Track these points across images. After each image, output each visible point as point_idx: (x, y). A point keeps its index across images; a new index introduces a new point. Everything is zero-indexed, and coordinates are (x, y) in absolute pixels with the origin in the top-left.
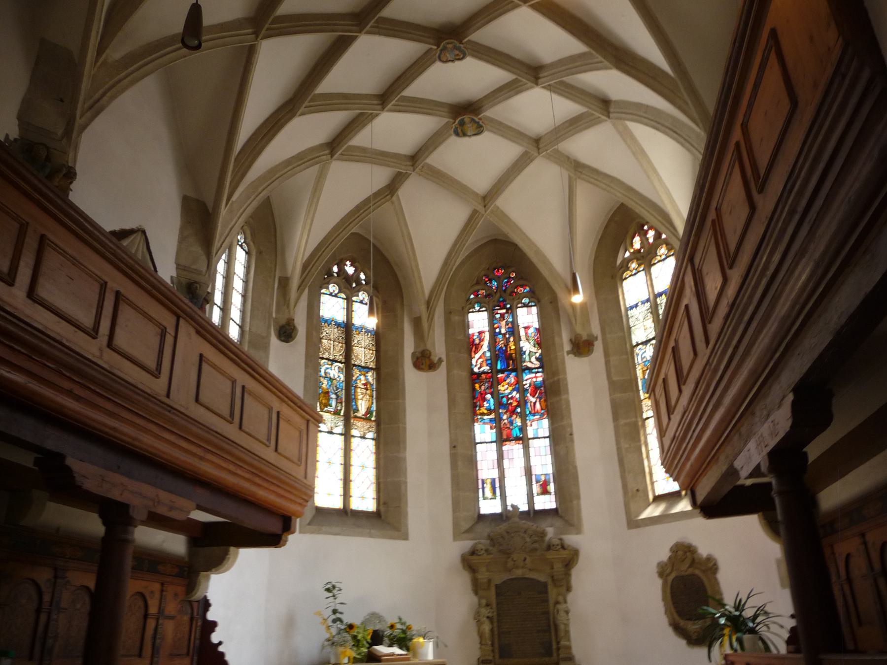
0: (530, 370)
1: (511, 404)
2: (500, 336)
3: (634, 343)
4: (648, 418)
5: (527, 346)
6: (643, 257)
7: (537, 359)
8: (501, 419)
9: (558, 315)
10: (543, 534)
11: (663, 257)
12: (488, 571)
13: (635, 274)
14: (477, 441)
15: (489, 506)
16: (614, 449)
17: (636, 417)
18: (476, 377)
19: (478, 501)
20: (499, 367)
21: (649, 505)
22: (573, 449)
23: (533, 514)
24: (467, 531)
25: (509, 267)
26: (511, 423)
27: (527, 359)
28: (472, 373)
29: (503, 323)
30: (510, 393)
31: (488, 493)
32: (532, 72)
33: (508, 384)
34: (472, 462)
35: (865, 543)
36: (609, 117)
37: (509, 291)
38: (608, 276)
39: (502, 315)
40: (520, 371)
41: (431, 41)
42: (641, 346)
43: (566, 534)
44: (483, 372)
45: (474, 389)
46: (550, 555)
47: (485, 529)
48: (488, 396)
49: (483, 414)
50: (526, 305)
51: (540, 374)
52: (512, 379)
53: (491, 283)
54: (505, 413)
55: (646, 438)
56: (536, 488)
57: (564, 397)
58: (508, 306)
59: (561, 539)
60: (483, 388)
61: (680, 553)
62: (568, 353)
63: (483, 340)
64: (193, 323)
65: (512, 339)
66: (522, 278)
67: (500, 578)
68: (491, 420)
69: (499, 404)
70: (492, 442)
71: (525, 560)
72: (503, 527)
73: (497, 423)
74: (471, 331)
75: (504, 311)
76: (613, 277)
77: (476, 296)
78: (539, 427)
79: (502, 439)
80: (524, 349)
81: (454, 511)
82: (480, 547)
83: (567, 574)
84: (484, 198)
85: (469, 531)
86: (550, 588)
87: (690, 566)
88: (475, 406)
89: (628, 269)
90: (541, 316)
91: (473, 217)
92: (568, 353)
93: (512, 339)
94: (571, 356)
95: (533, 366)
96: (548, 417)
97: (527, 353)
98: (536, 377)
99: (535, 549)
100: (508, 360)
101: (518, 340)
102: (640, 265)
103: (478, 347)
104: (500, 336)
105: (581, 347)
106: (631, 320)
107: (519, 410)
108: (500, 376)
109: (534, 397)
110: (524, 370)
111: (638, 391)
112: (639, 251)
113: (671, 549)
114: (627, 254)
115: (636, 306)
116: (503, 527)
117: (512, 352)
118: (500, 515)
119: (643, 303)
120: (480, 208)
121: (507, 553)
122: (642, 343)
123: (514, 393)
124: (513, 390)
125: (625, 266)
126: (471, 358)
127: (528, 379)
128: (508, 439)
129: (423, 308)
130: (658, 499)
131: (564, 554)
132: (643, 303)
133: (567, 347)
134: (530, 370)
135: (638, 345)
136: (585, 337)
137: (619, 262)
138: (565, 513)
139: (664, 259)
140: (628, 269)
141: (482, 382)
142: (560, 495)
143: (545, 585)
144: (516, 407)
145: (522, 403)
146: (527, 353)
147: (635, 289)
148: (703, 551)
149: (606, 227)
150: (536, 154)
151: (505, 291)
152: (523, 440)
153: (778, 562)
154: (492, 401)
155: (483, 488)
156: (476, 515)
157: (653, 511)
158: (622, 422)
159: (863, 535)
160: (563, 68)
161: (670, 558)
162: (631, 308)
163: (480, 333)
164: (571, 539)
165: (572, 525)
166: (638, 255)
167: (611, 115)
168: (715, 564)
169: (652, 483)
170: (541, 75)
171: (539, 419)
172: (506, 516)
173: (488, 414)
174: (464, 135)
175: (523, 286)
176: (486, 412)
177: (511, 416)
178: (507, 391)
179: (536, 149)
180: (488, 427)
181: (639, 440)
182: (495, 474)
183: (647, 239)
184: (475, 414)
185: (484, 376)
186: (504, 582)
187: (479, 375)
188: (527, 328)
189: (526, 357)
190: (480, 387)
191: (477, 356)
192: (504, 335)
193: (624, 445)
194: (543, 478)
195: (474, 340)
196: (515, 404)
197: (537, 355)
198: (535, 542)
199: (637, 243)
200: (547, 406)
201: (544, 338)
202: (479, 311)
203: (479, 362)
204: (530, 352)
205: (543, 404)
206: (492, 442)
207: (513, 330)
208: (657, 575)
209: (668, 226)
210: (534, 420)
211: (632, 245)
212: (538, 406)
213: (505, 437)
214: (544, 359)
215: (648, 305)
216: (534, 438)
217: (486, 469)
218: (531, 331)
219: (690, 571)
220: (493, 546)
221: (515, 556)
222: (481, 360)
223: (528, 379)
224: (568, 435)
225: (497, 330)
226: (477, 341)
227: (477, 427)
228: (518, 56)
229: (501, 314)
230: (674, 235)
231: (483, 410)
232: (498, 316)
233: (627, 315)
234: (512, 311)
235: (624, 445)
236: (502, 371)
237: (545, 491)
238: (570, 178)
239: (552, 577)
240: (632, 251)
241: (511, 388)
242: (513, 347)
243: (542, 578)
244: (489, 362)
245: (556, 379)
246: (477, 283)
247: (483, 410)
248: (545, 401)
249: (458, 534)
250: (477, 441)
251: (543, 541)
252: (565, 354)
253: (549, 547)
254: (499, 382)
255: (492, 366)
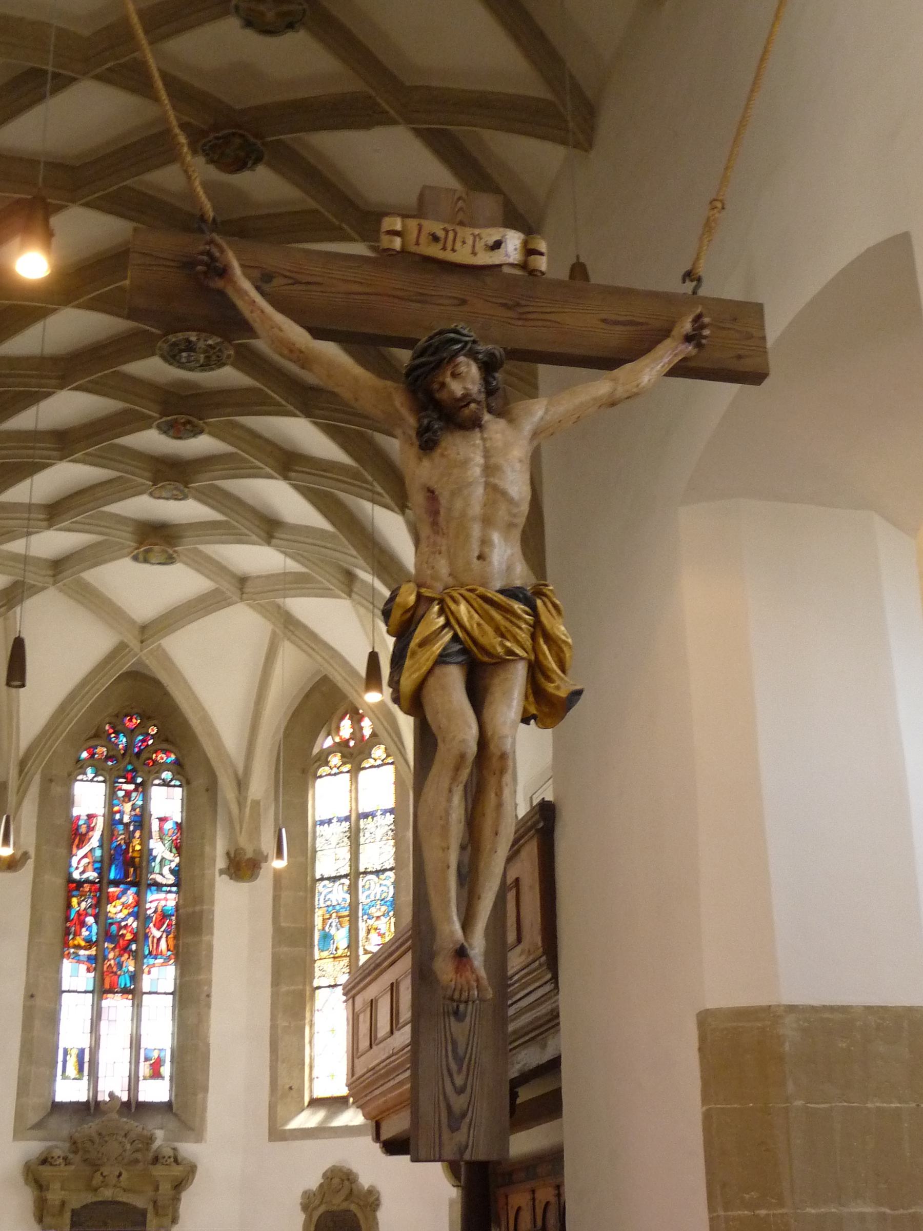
0: (158, 886)
1: (123, 936)
2: (121, 827)
3: (318, 876)
4: (319, 988)
5: (159, 849)
6: (352, 754)
7: (172, 871)
8: (105, 958)
9: (215, 812)
10: (151, 1139)
11: (379, 762)
12: (62, 1188)
13: (335, 774)
14: (64, 988)
15: (70, 1090)
16: (268, 1024)
17: (304, 985)
18: (74, 886)
19: (55, 1080)
20: (112, 876)
21: (303, 1110)
22: (208, 1020)
23: (134, 1108)
24: (34, 1127)
25: (149, 718)
26: (120, 965)
27: (157, 870)
28: (70, 880)
29: (127, 807)
30: (123, 919)
31: (72, 1070)
32: (270, 528)
33: (123, 904)
34: (53, 1019)
35: (534, 1199)
36: (350, 596)
37: (144, 756)
38: (298, 767)
39: (128, 794)
40: (143, 886)
41: (147, 474)
42: (326, 882)
43: (181, 1141)
44: (87, 881)
45: (69, 906)
46: (158, 1171)
47: (64, 1127)
48: (90, 920)
49: (79, 947)
50: (166, 784)
51: (173, 896)
52: (130, 897)
53: (117, 737)
54: (113, 949)
55: (312, 1015)
56: (144, 1069)
57: (205, 938)
58: (139, 780)
59: (175, 1149)
60: (83, 905)
61: (336, 1181)
62: (222, 872)
63: (93, 829)
64: (133, 1067)
65: (137, 834)
66: (167, 740)
67: (80, 1199)
68: (89, 958)
69: (107, 935)
70: (86, 992)
71: (120, 1175)
72: (92, 1127)
73: (96, 963)
74: (76, 812)
75: (131, 787)
76: (304, 771)
77: (92, 755)
78: (161, 977)
79: (103, 988)
80: (154, 853)
81: (19, 1095)
82: (57, 1153)
83: (176, 1199)
84: (144, 628)
85: (39, 1125)
86: (150, 1215)
87: (346, 1199)
88: (67, 932)
89: (326, 763)
90: (189, 804)
91: (120, 649)
92: (222, 872)
93: (137, 834)
94: (225, 877)
95: (164, 881)
96: (176, 963)
97: (158, 860)
98: (166, 899)
99: (137, 1161)
100: (126, 864)
101: (146, 836)
102: (344, 763)
103: (82, 839)
104: (121, 827)
105: (243, 867)
106: (318, 841)
107: (134, 947)
108: (111, 890)
109: (159, 929)
110: (150, 886)
111: (312, 946)
112: (348, 741)
113: (324, 1175)
114: (329, 742)
115: (329, 822)
116: (92, 1127)
117: (135, 855)
118: (127, 1105)
119: (340, 820)
120: (134, 644)
121: (95, 1165)
122: (329, 879)
123: (130, 920)
124: (130, 914)
125: (323, 759)
126: (71, 855)
127: (156, 901)
128: (111, 991)
129: (13, 772)
130: (316, 1103)
131: (177, 1171)
132: (340, 820)
133: (221, 863)
134: (158, 886)
135: (322, 879)
136: (249, 854)
137: (316, 750)
138: (183, 1111)
139: (378, 766)
140: (326, 763)
141: (82, 896)
142: (180, 1081)
143: (144, 1213)
144: (130, 941)
145: (141, 937)
146: (158, 860)
147: (329, 794)
148: (365, 1181)
149: (307, 696)
150: (235, 598)
151: (138, 755)
152: (133, 992)
153: (452, 1203)
154: (95, 928)
155: (65, 1062)
156: (50, 1104)
157: (308, 1119)
158: (284, 988)
159: (533, 1192)
160: (310, 541)
161: (321, 1185)
162: (322, 823)
163: (90, 817)
164: (188, 1149)
165: (191, 1129)
166: (345, 750)
167: (354, 595)
168: (378, 1199)
169: (311, 1080)
170: (276, 535)
171: (162, 965)
172: (89, 1109)
173: (85, 948)
174: (146, 561)
175: (167, 752)
176: (83, 943)
177: (121, 955)
178: (121, 915)
179: (239, 593)
180: (83, 968)
181: (304, 1018)
182: (85, 1042)
183: (362, 728)
184: (66, 944)
185: (87, 887)
186: (85, 1207)
187: (80, 884)
188: (162, 820)
189: (156, 865)
190: (79, 904)
191: (81, 852)
192: (127, 825)
193: (282, 1023)
194: (155, 1055)
195: (78, 827)
196: (129, 937)
197: (173, 865)
198: (137, 1151)
199: (346, 728)
200: (176, 946)
201: (185, 840)
202: (92, 781)
203: (81, 864)
204: (163, 859)
205: (171, 942)
206: (86, 992)
207: (141, 820)
208: (299, 1207)
209: (396, 739)
210: (154, 965)
211: (338, 729)
212: (163, 945)
213: (107, 986)
214: (183, 875)
215: (346, 825)
216: (150, 993)
217: (72, 1031)
218: (169, 825)
219: (345, 1206)
220: (76, 1152)
221: (106, 1170)
222: (86, 861)
223: (156, 901)
224: (203, 996)
225: (118, 816)
226: (83, 830)
227: (67, 965)
228: (250, 502)
229: (126, 791)
230: (401, 753)
231: (80, 941)
232: (121, 794)
233: (314, 832)
234: (143, 788)
235: (282, 1023)
236: (116, 883)
237: (156, 1074)
238: (274, 635)
239: (155, 1202)
240: (337, 740)
241: (126, 912)
242: (138, 848)
243: (139, 1202)
244: (98, 865)
245: (198, 908)
246: (96, 736)
247: (80, 941)
248: (175, 938)
249: (19, 1133)
250: (64, 988)
251: (148, 1149)
252: (217, 874)
253: (156, 1160)
254: (110, 899)
255: (101, 872)
